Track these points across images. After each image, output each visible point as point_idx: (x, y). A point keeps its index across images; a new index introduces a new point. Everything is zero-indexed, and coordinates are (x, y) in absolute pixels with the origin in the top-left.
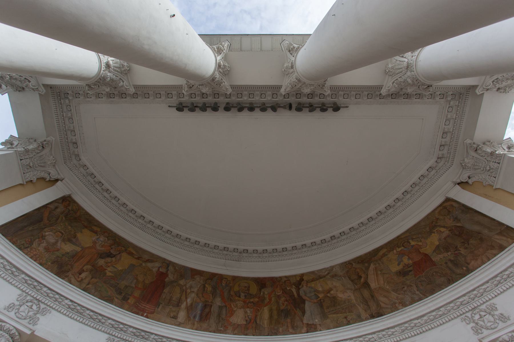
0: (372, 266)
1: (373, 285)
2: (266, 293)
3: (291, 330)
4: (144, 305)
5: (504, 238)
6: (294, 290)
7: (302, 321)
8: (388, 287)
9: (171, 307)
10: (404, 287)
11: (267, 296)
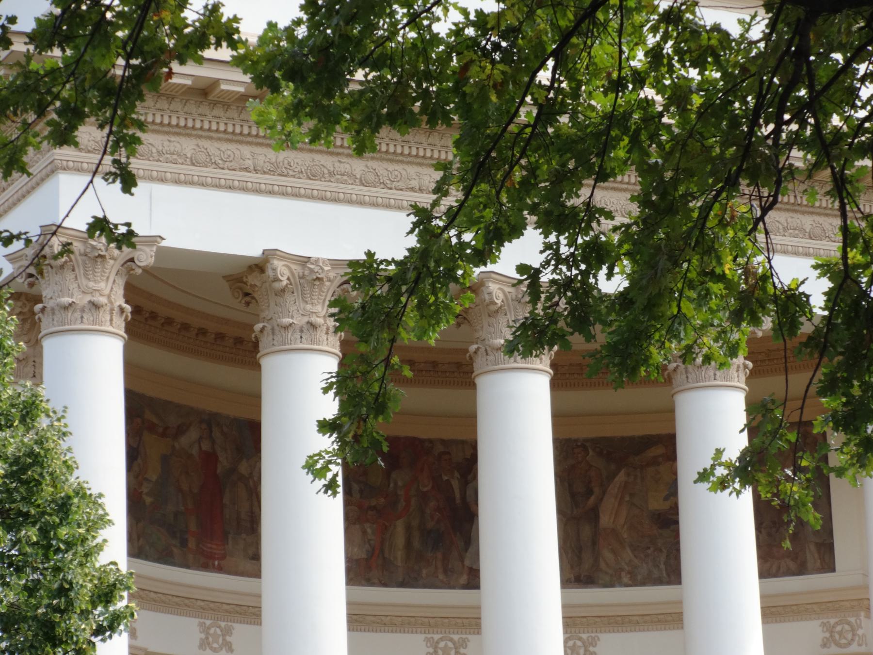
0: (621, 477)
1: (605, 520)
2: (400, 484)
3: (441, 576)
4: (209, 545)
5: (816, 555)
6: (455, 484)
7: (462, 561)
8: (625, 536)
9: (244, 536)
10: (649, 548)
11: (401, 492)
